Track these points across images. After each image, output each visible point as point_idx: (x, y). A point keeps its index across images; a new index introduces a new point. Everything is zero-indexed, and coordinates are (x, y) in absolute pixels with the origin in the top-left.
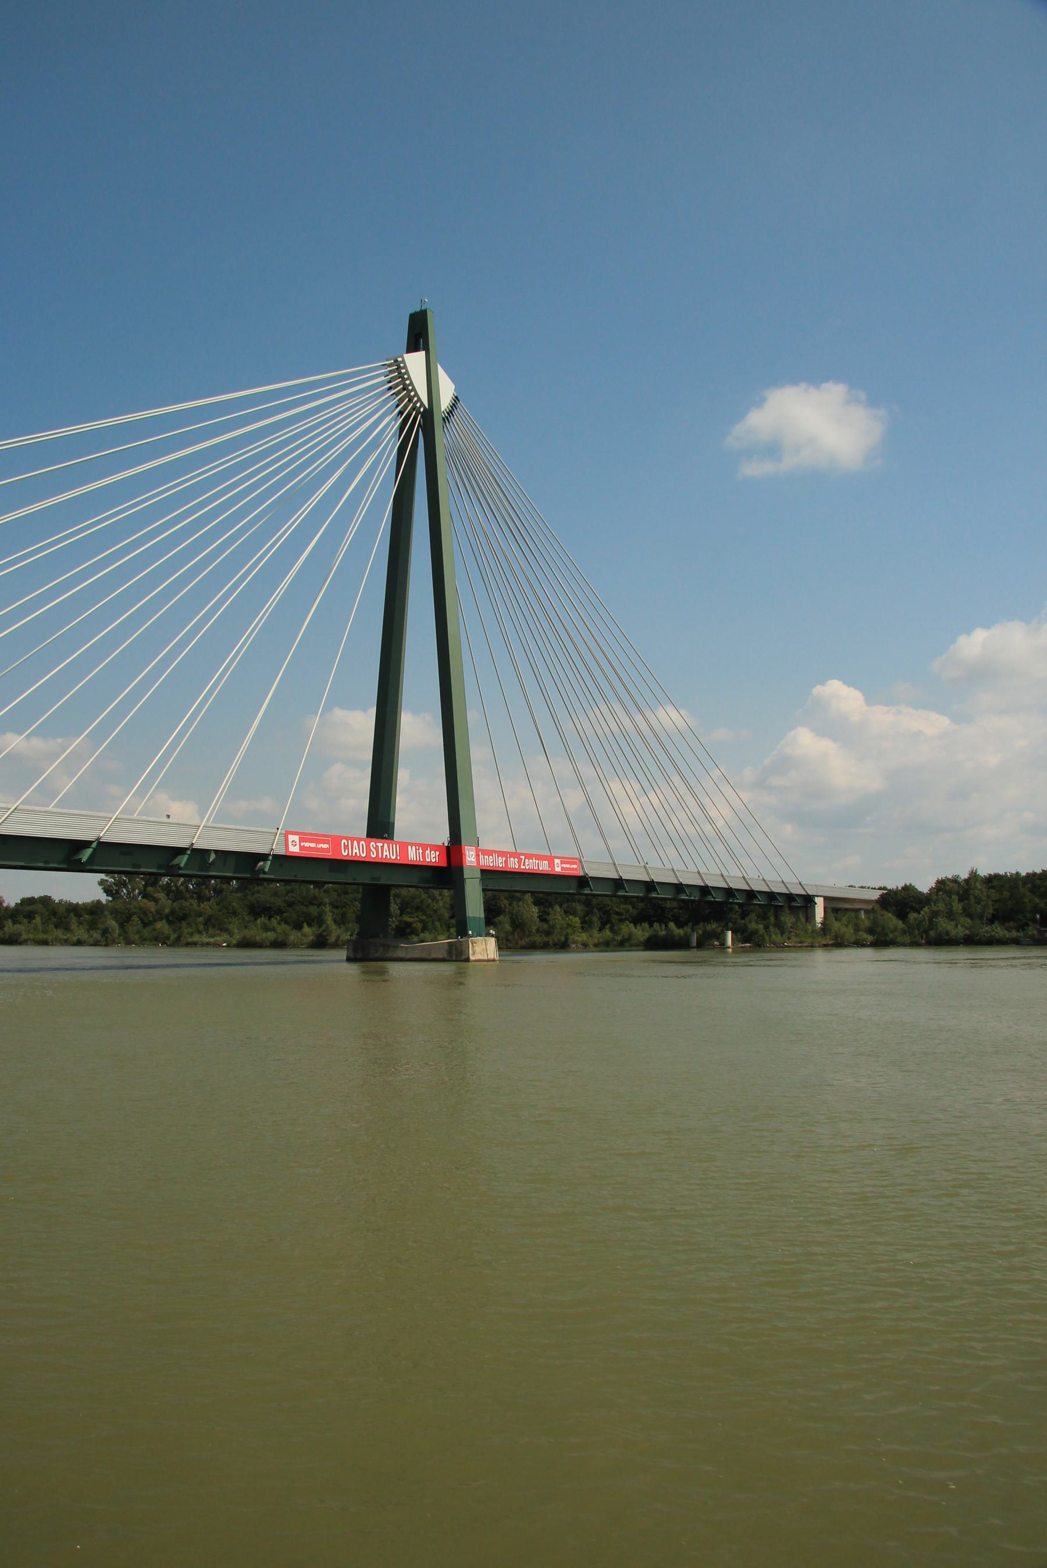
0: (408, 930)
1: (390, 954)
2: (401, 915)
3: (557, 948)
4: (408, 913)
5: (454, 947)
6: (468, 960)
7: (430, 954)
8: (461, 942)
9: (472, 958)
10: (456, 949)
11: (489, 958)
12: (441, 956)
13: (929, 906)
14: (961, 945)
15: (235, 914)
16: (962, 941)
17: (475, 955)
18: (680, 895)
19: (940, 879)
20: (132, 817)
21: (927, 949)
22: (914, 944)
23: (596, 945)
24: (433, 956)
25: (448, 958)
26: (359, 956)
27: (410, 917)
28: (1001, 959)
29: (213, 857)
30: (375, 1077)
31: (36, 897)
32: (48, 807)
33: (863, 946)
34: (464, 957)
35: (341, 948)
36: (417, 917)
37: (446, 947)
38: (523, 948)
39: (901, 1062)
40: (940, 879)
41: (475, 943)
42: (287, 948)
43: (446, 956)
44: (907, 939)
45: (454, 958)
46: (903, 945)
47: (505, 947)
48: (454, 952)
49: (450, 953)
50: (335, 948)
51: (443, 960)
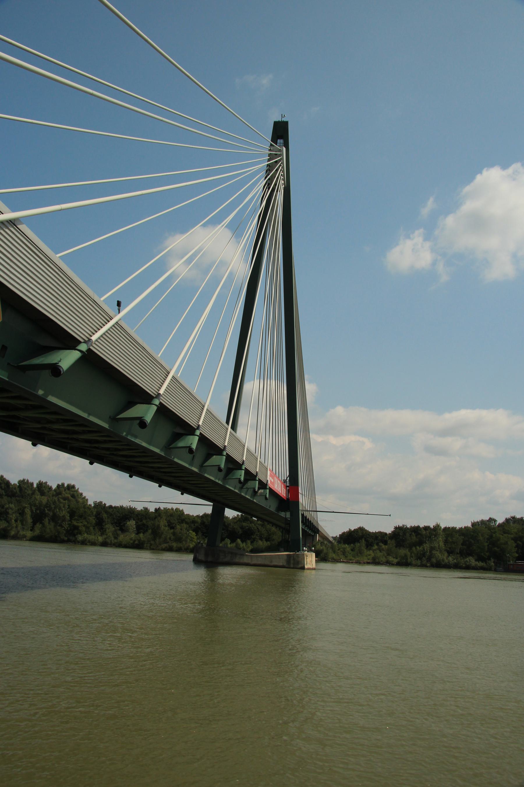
0: (76, 531)
1: (237, 560)
2: (70, 521)
3: (187, 552)
6: (303, 568)
7: (271, 562)
8: (297, 554)
9: (306, 567)
11: (313, 567)
12: (281, 564)
14: (452, 569)
16: (453, 566)
17: (307, 565)
18: (267, 498)
20: (96, 298)
21: (431, 569)
22: (423, 566)
23: (355, 562)
25: (287, 566)
26: (210, 559)
27: (77, 523)
29: (194, 442)
30: (272, 606)
31: (421, 527)
32: (57, 253)
34: (300, 566)
35: (21, 540)
36: (81, 523)
41: (307, 556)
42: (7, 539)
43: (285, 564)
44: (419, 562)
45: (292, 566)
46: (416, 566)
47: (149, 548)
48: (292, 562)
50: (63, 543)
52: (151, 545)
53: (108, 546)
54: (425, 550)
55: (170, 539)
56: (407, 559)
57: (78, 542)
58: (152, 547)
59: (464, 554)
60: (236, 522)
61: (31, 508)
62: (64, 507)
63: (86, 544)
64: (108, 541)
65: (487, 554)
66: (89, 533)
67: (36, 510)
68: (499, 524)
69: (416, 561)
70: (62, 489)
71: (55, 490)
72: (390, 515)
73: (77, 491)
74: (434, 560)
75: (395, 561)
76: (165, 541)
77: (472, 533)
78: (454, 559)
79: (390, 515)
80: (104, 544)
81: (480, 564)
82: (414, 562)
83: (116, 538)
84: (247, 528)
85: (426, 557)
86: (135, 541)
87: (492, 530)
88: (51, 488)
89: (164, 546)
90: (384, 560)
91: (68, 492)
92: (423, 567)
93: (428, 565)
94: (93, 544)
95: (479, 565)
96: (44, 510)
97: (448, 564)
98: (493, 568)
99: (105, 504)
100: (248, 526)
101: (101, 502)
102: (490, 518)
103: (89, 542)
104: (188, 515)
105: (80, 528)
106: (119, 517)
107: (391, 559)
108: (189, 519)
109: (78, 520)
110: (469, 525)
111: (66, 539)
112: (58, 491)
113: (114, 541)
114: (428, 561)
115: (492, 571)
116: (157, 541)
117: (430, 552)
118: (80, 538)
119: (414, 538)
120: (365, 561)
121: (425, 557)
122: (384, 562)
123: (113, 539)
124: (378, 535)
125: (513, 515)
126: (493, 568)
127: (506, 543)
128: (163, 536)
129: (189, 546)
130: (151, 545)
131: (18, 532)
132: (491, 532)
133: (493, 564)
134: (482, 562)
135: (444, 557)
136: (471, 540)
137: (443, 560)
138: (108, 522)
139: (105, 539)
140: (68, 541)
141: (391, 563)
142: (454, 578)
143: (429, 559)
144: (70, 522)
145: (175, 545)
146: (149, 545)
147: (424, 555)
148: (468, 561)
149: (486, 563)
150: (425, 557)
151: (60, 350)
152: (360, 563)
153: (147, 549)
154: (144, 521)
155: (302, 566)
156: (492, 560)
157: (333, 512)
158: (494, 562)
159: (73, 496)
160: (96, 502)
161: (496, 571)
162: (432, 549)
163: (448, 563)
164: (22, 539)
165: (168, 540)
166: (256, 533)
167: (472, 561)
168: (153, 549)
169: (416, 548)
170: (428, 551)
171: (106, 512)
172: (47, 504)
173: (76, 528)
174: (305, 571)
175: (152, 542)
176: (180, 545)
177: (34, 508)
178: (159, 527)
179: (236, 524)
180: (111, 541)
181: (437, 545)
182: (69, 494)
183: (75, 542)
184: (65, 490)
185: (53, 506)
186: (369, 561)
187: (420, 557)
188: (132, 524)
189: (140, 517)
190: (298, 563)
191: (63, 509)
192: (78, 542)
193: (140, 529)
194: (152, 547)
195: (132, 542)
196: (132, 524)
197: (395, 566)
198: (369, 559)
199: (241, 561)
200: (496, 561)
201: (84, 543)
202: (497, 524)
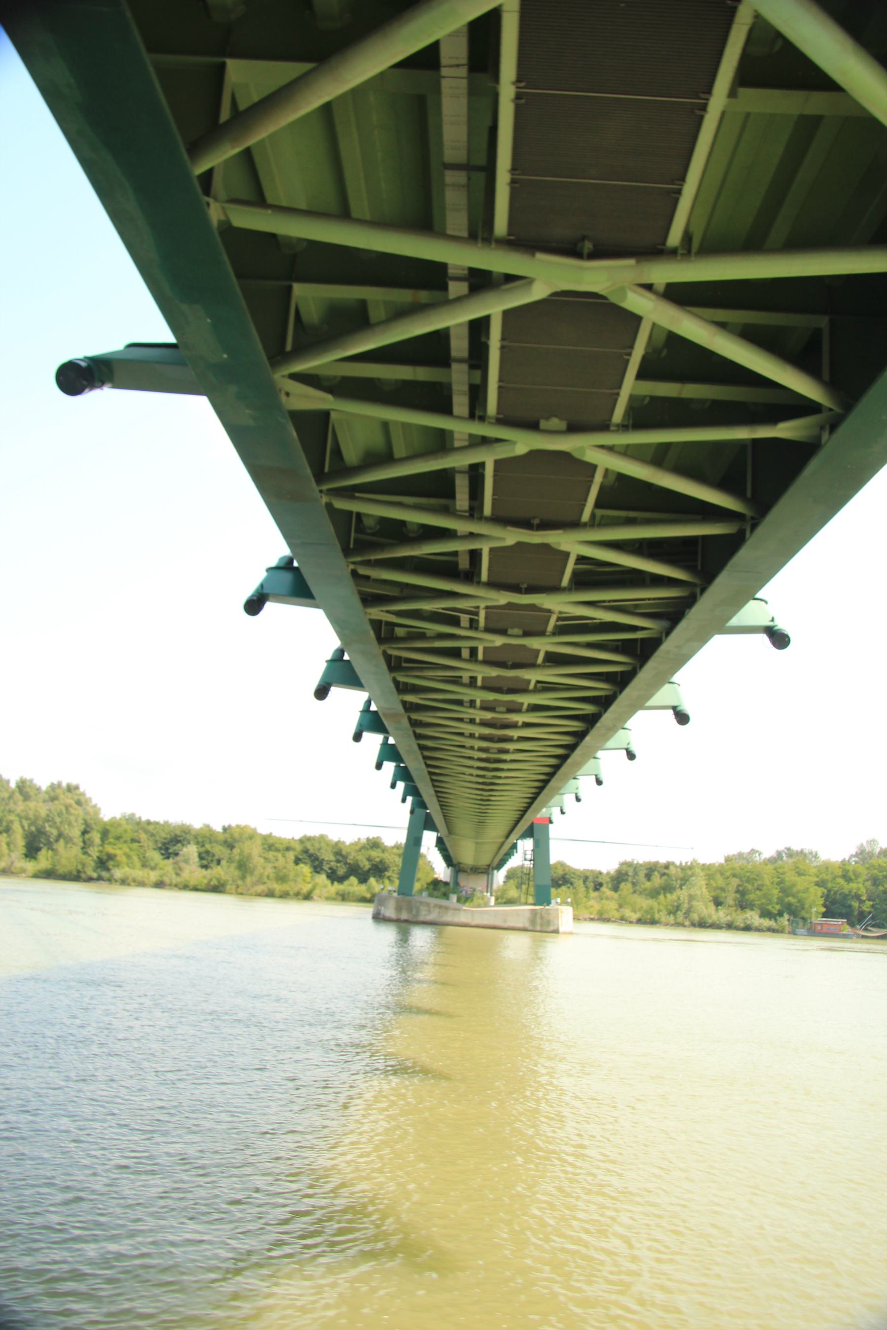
2: (102, 845)
3: (299, 899)
4: (110, 843)
5: (538, 916)
6: (556, 931)
7: (505, 921)
8: (547, 910)
9: (561, 930)
10: (542, 917)
12: (521, 925)
13: (860, 909)
15: (811, 923)
19: (684, 864)
24: (510, 924)
25: (530, 928)
26: (404, 916)
27: (113, 849)
28: (671, 940)
33: (607, 920)
34: (551, 928)
35: (18, 876)
36: (120, 849)
37: (528, 915)
38: (259, 895)
39: (209, 1105)
40: (684, 864)
43: (527, 925)
44: (671, 919)
47: (234, 891)
48: (538, 921)
49: (533, 921)
51: (524, 930)
52: (238, 887)
53: (22, 876)
54: (680, 900)
55: (268, 877)
56: (654, 913)
57: (116, 881)
58: (240, 890)
59: (743, 905)
60: (360, 850)
61: (21, 822)
62: (76, 821)
63: (129, 885)
64: (167, 880)
65: (778, 907)
66: (131, 865)
67: (30, 825)
68: (765, 859)
69: (667, 916)
70: (58, 791)
71: (47, 792)
72: (692, 848)
73: (83, 794)
74: (695, 917)
75: (635, 917)
76: (260, 881)
77: (748, 874)
78: (727, 915)
79: (692, 848)
80: (159, 885)
81: (766, 923)
82: (663, 919)
83: (177, 874)
84: (378, 860)
85: (684, 911)
86: (211, 880)
87: (779, 870)
88: (39, 789)
89: (260, 888)
90: (617, 915)
91: (69, 795)
92: (678, 926)
93: (687, 923)
94: (141, 884)
95: (765, 924)
96: (44, 827)
97: (718, 922)
98: (787, 929)
99: (140, 818)
100: (379, 857)
101: (133, 815)
102: (752, 850)
103: (134, 881)
104: (275, 836)
105: (118, 858)
106: (165, 839)
107: (628, 913)
108: (281, 844)
109: (115, 845)
110: (722, 861)
111: (95, 875)
112: (52, 794)
113: (175, 880)
114: (686, 918)
115: (786, 933)
116: (249, 880)
117: (689, 902)
118: (118, 873)
119: (657, 881)
120: (587, 916)
121: (681, 911)
122: (617, 919)
123: (174, 876)
124: (588, 875)
125: (129, 812)
126: (787, 929)
127: (806, 890)
128: (257, 873)
129: (301, 889)
130: (238, 887)
131: (12, 863)
132: (778, 872)
133: (787, 923)
134: (770, 919)
135: (705, 909)
136: (747, 884)
137: (710, 916)
138: (148, 846)
139: (161, 876)
140: (100, 878)
141: (629, 920)
142: (718, 942)
143: (687, 914)
144: (101, 848)
145: (278, 887)
146: (234, 887)
147: (678, 908)
148: (749, 918)
149: (776, 920)
150: (681, 911)
151: (803, 440)
152: (579, 920)
153: (232, 894)
154: (208, 846)
155: (555, 928)
156: (786, 916)
157: (603, 842)
158: (789, 920)
159: (79, 803)
160: (125, 813)
161: (793, 933)
162: (691, 898)
163: (718, 920)
164: (20, 875)
165: (265, 879)
166: (392, 869)
167: (753, 917)
168: (242, 894)
169: (665, 897)
170: (686, 901)
171: (146, 832)
172: (48, 815)
173: (111, 857)
174: (559, 935)
175: (240, 882)
176: (285, 887)
177: (26, 824)
178: (249, 857)
179: (360, 853)
180: (171, 880)
181: (699, 892)
182: (72, 798)
183: (795, 934)
184: (64, 793)
185: (58, 820)
186: (592, 916)
187: (674, 910)
188: (191, 851)
189: (200, 840)
190: (549, 923)
191: (75, 824)
192: (116, 881)
193: (206, 860)
194: (240, 890)
195: (205, 881)
196: (191, 851)
197: (649, 926)
198: (591, 914)
199: (456, 919)
200: (792, 918)
201: (124, 882)
202: (763, 858)
